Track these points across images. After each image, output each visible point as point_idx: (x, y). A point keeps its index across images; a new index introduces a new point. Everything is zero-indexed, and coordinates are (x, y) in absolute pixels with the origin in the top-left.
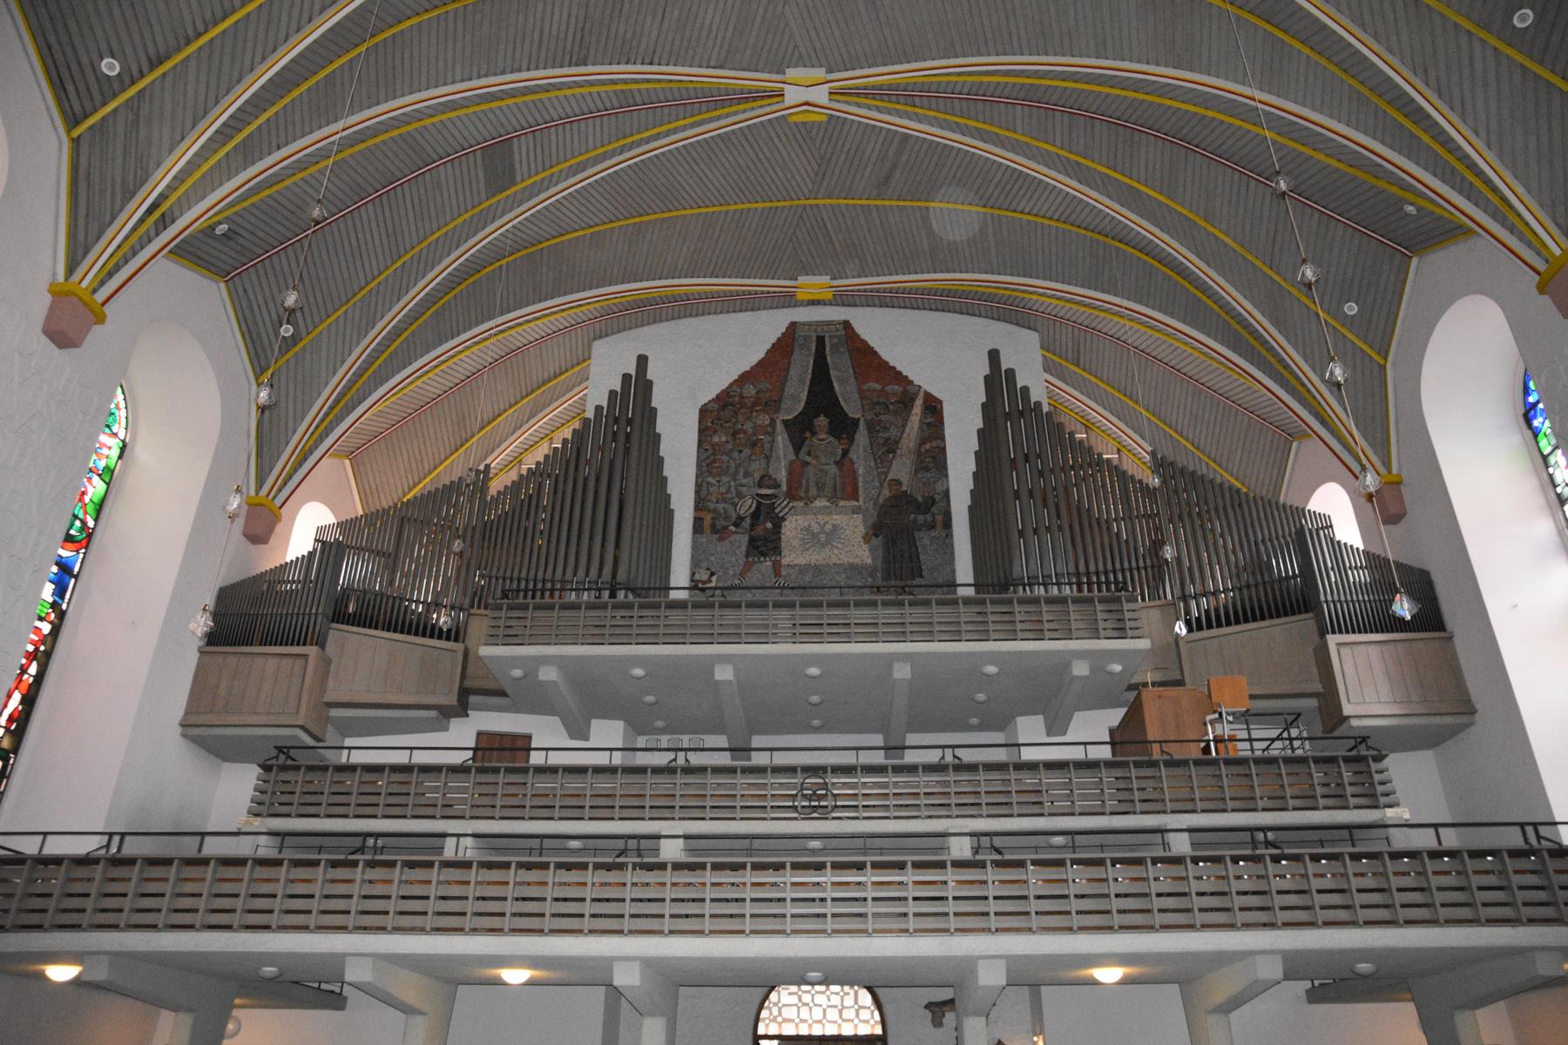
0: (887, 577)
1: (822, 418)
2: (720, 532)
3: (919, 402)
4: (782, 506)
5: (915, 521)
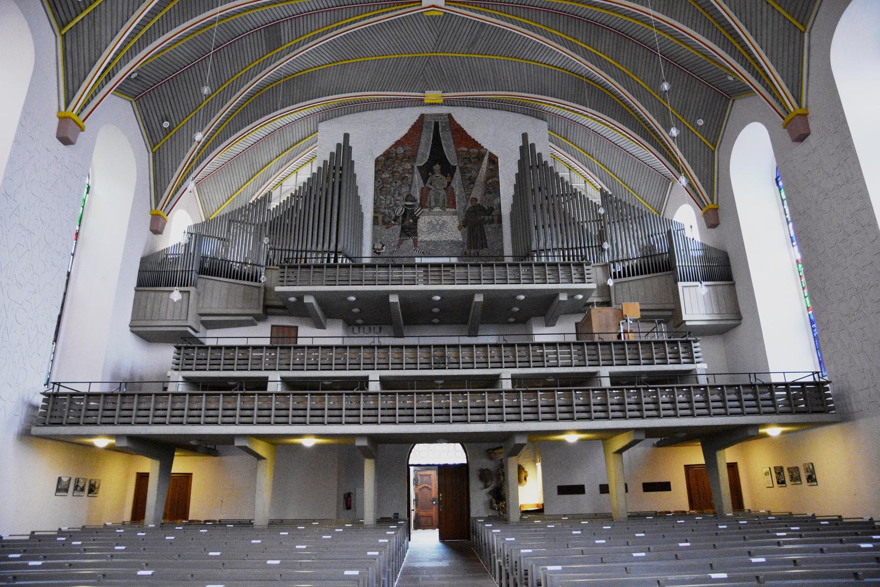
0: (470, 248)
1: (437, 165)
2: (387, 224)
3: (486, 158)
4: (418, 210)
5: (484, 219)
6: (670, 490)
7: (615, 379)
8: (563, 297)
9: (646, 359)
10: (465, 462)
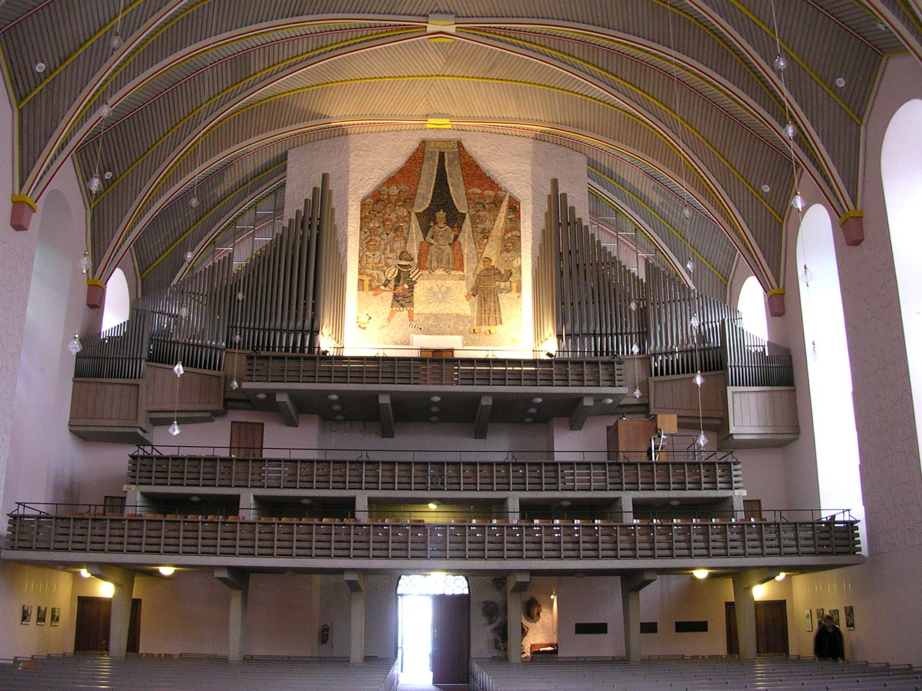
2: (374, 289)
3: (505, 204)
4: (414, 273)
6: (706, 630)
7: (640, 508)
8: (588, 402)
10: (466, 592)
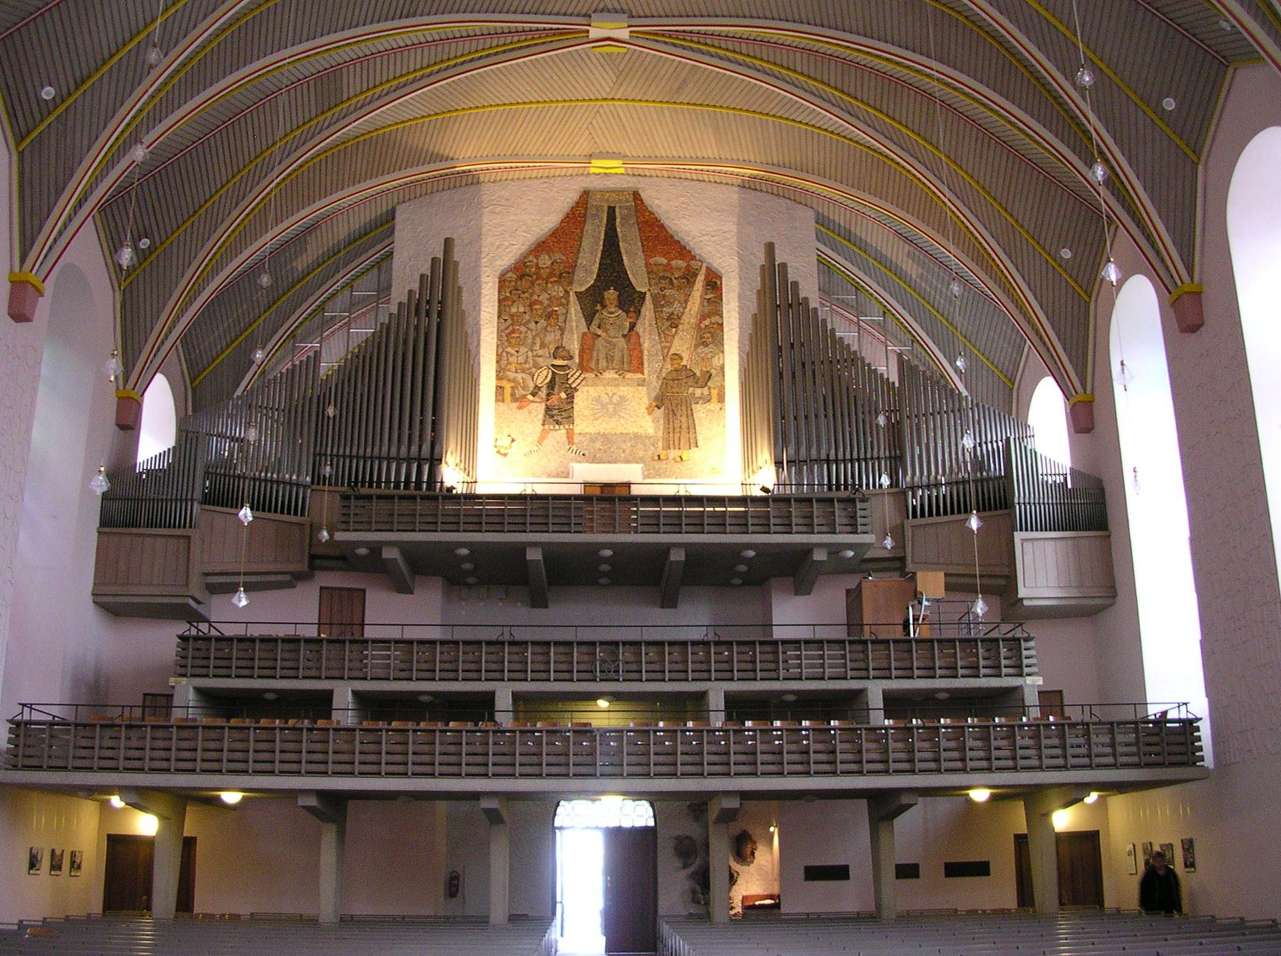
2: (519, 400)
3: (701, 278)
4: (574, 377)
6: (988, 874)
9: (946, 668)
10: (651, 823)
